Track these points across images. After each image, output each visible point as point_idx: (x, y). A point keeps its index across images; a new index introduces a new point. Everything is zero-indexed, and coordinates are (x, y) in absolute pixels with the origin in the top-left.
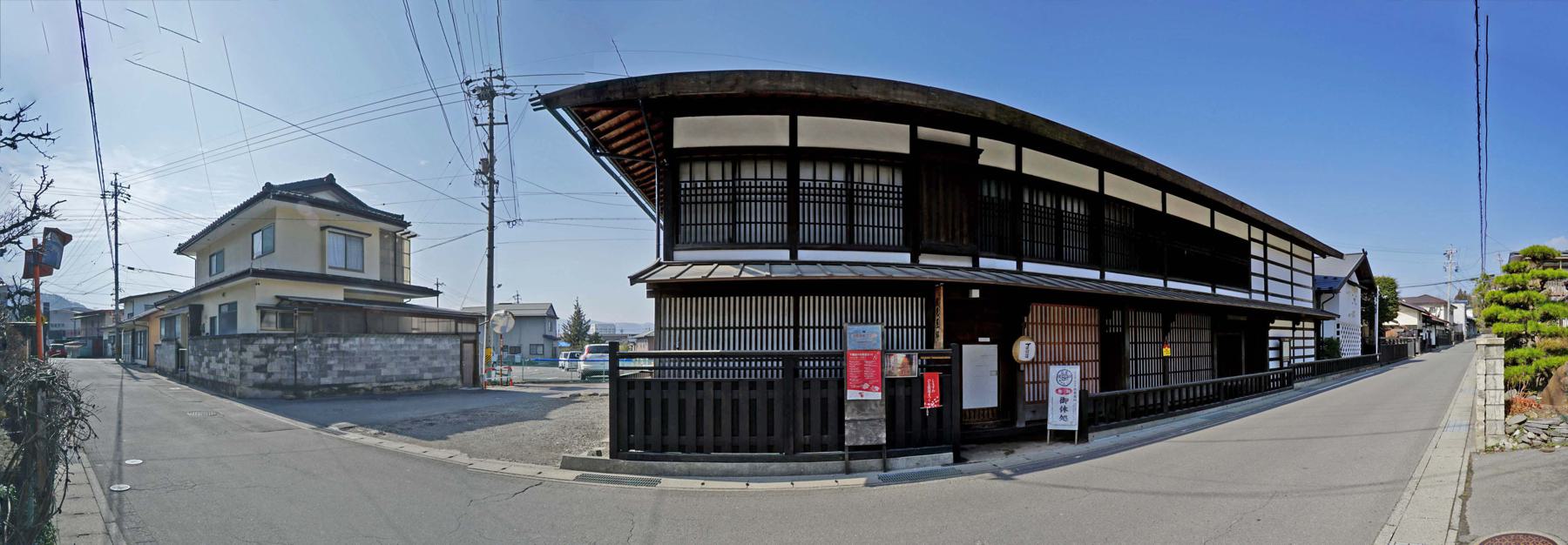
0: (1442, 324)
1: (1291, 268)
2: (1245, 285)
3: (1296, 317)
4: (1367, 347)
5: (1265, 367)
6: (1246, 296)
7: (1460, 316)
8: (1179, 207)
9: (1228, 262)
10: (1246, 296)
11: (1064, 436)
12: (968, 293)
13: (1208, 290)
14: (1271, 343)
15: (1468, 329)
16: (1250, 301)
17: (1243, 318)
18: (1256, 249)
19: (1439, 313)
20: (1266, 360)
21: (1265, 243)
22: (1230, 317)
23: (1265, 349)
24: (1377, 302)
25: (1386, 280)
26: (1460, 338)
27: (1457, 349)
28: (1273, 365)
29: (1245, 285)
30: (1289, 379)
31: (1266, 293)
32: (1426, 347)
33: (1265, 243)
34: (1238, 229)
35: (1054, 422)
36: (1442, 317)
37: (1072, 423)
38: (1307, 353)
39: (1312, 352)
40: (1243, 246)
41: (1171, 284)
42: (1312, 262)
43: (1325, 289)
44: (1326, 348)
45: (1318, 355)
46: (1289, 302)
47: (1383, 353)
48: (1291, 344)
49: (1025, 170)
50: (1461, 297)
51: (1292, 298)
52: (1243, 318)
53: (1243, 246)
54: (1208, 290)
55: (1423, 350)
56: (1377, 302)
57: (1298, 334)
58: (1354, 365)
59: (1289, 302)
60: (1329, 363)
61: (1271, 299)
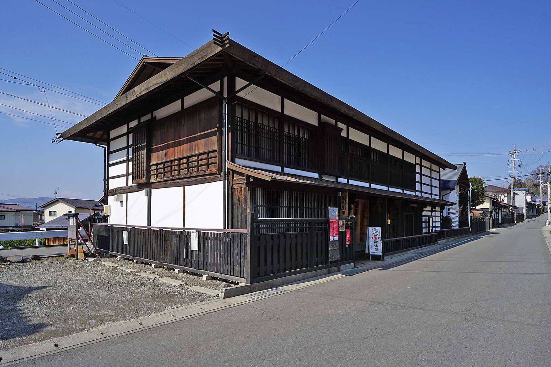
0: (506, 207)
1: (431, 177)
2: (413, 189)
3: (434, 205)
4: (463, 221)
5: (421, 232)
6: (413, 194)
7: (521, 200)
8: (379, 145)
9: (404, 175)
10: (413, 194)
11: (377, 258)
12: (338, 194)
13: (401, 191)
14: (424, 219)
15: (528, 210)
16: (416, 196)
17: (415, 206)
18: (418, 169)
19: (504, 199)
20: (421, 228)
21: (421, 165)
22: (412, 205)
23: (421, 222)
24: (470, 194)
25: (475, 179)
26: (521, 218)
27: (518, 227)
28: (424, 231)
29: (413, 189)
30: (432, 239)
31: (421, 192)
32: (496, 224)
33: (421, 165)
34: (410, 158)
35: (373, 252)
36: (506, 201)
37: (380, 252)
38: (436, 225)
39: (438, 224)
40: (413, 166)
41: (391, 189)
42: (439, 172)
43: (445, 186)
44: (446, 221)
45: (442, 227)
46: (429, 196)
47: (473, 228)
48: (432, 220)
49: (286, 113)
50: (519, 185)
51: (431, 194)
52: (415, 206)
53: (413, 166)
54: (401, 191)
55: (494, 227)
56: (470, 194)
57: (434, 214)
58: (456, 233)
59: (429, 196)
60: (447, 234)
61: (424, 195)
